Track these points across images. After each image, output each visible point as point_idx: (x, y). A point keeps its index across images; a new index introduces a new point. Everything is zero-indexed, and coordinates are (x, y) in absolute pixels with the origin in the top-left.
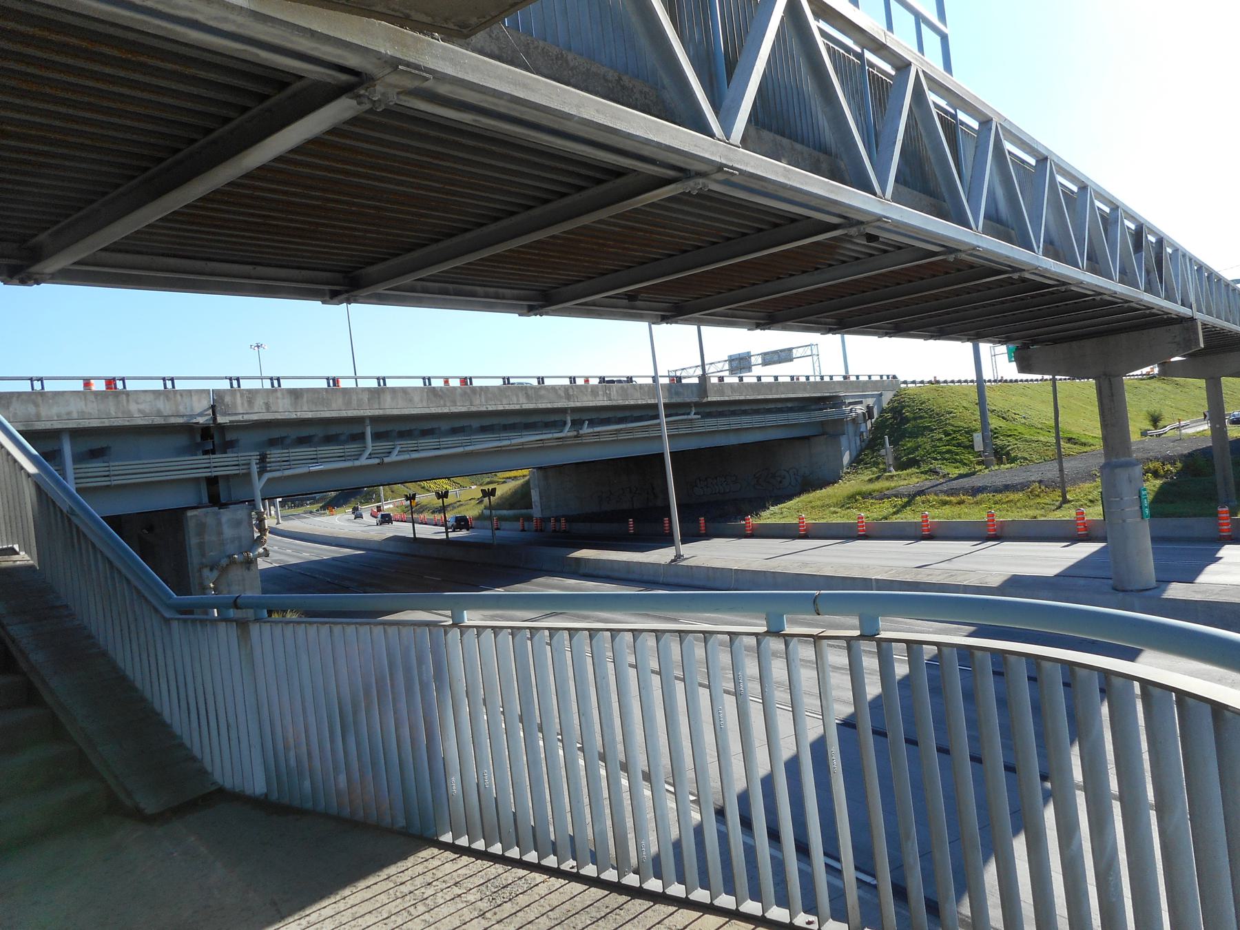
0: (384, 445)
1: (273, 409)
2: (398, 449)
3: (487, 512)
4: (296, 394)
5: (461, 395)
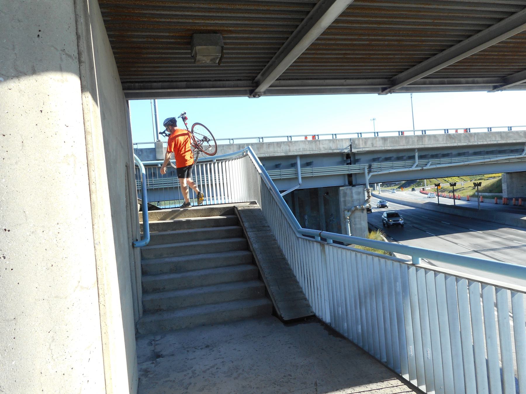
0: (424, 161)
1: (375, 146)
2: (430, 163)
3: (476, 193)
4: (385, 139)
5: (464, 137)
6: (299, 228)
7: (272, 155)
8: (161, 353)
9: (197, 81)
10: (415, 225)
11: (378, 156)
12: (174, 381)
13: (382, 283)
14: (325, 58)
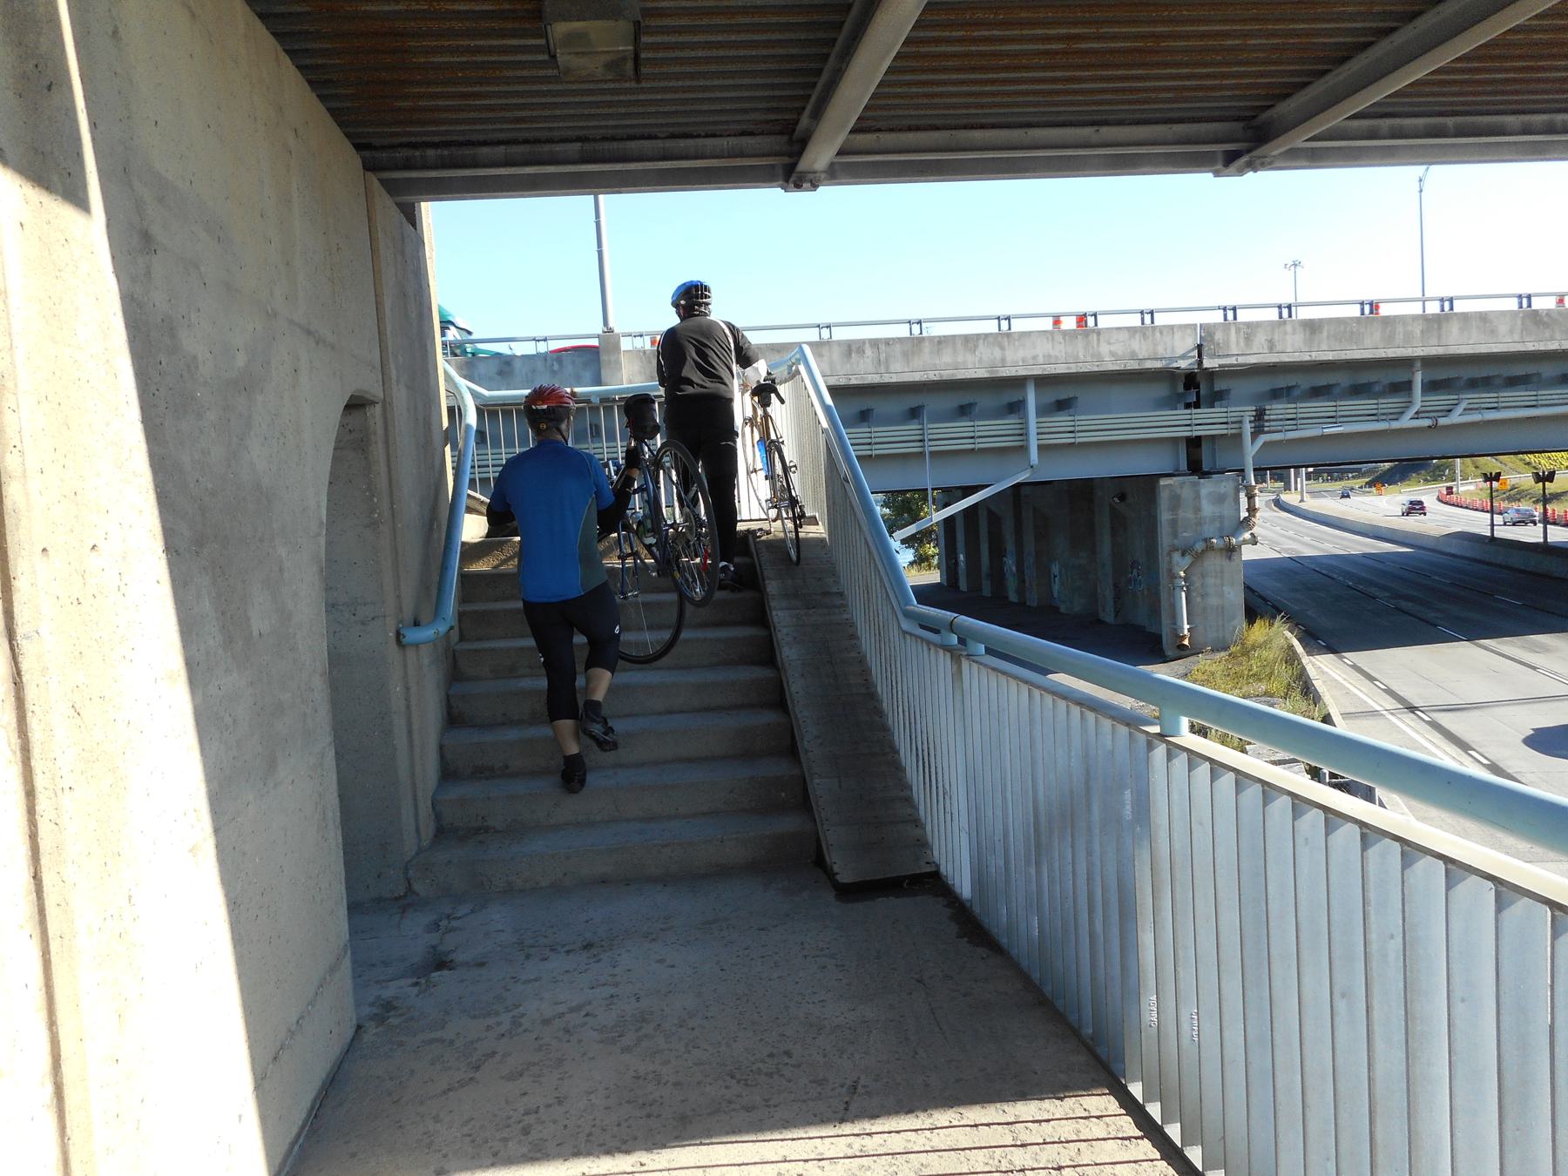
0: (1440, 400)
1: (1279, 348)
2: (1464, 405)
4: (1312, 327)
6: (908, 602)
7: (947, 375)
8: (452, 956)
9: (613, 139)
10: (1404, 604)
11: (1286, 382)
12: (452, 1042)
13: (1088, 789)
14: (1008, 55)
